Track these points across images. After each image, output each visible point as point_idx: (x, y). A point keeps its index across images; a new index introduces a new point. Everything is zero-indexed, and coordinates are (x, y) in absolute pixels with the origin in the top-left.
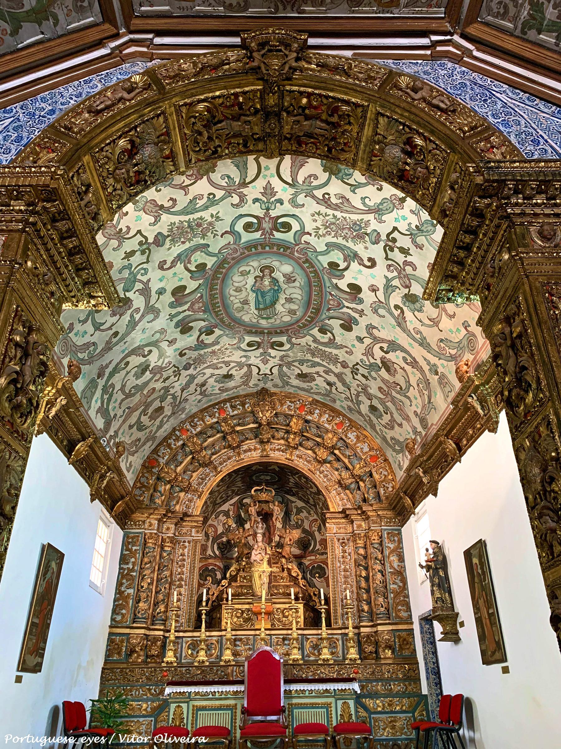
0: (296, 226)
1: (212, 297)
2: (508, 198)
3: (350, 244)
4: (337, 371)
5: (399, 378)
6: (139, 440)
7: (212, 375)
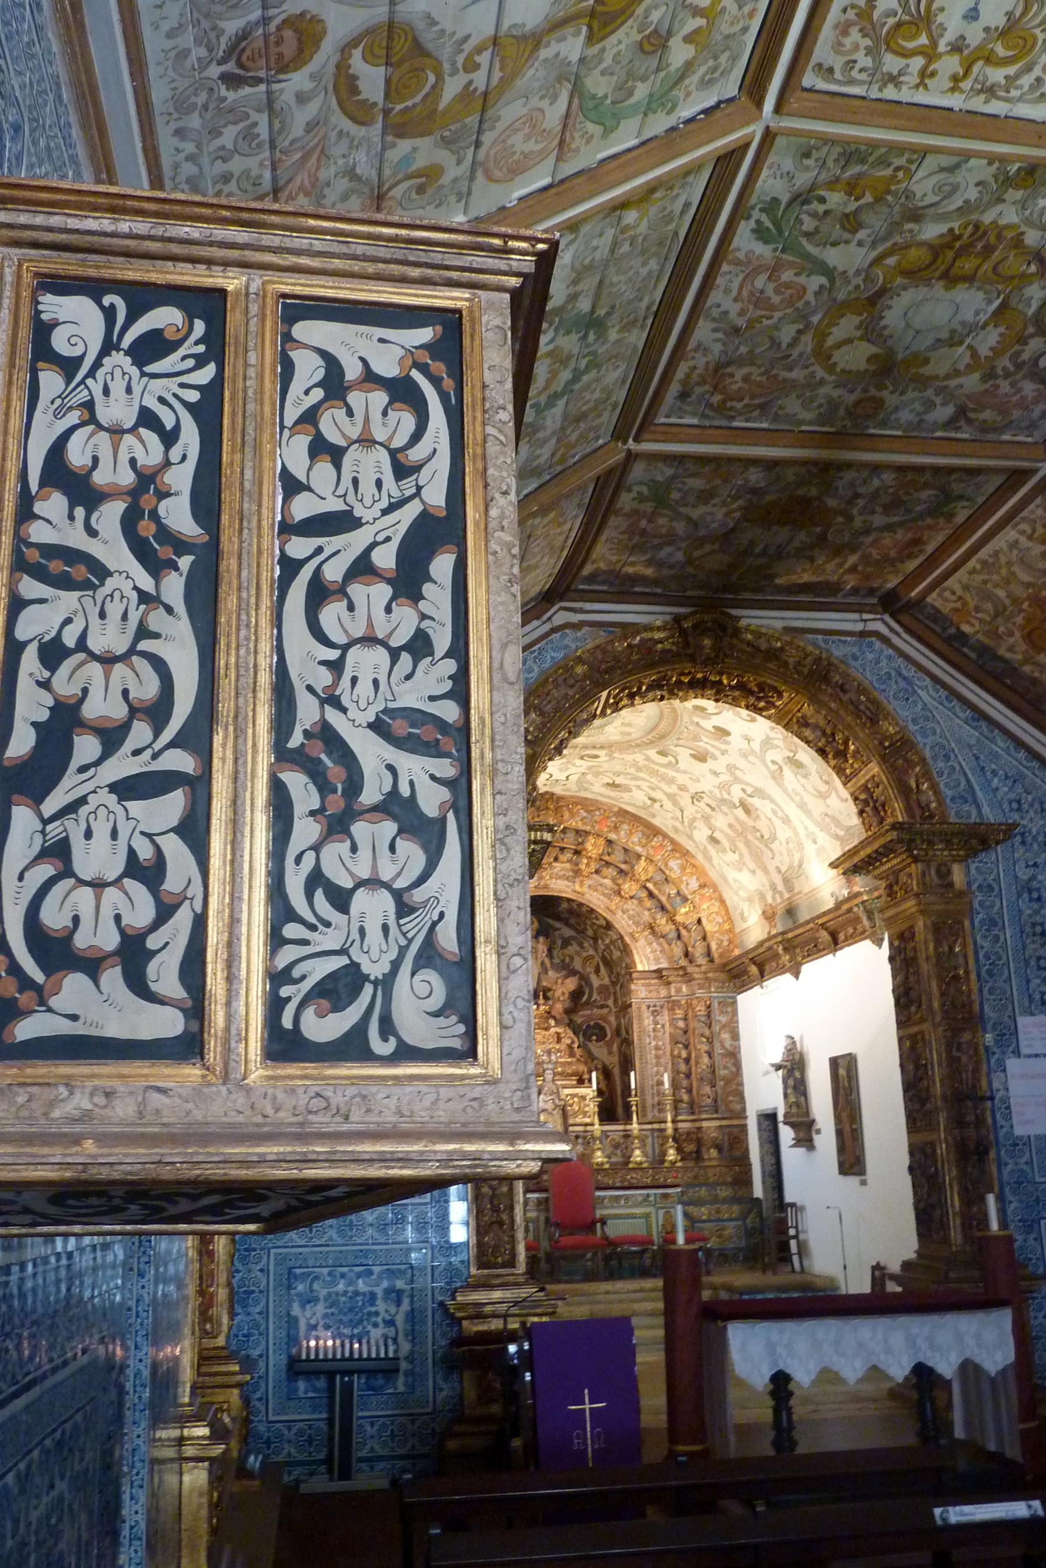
5: (763, 825)
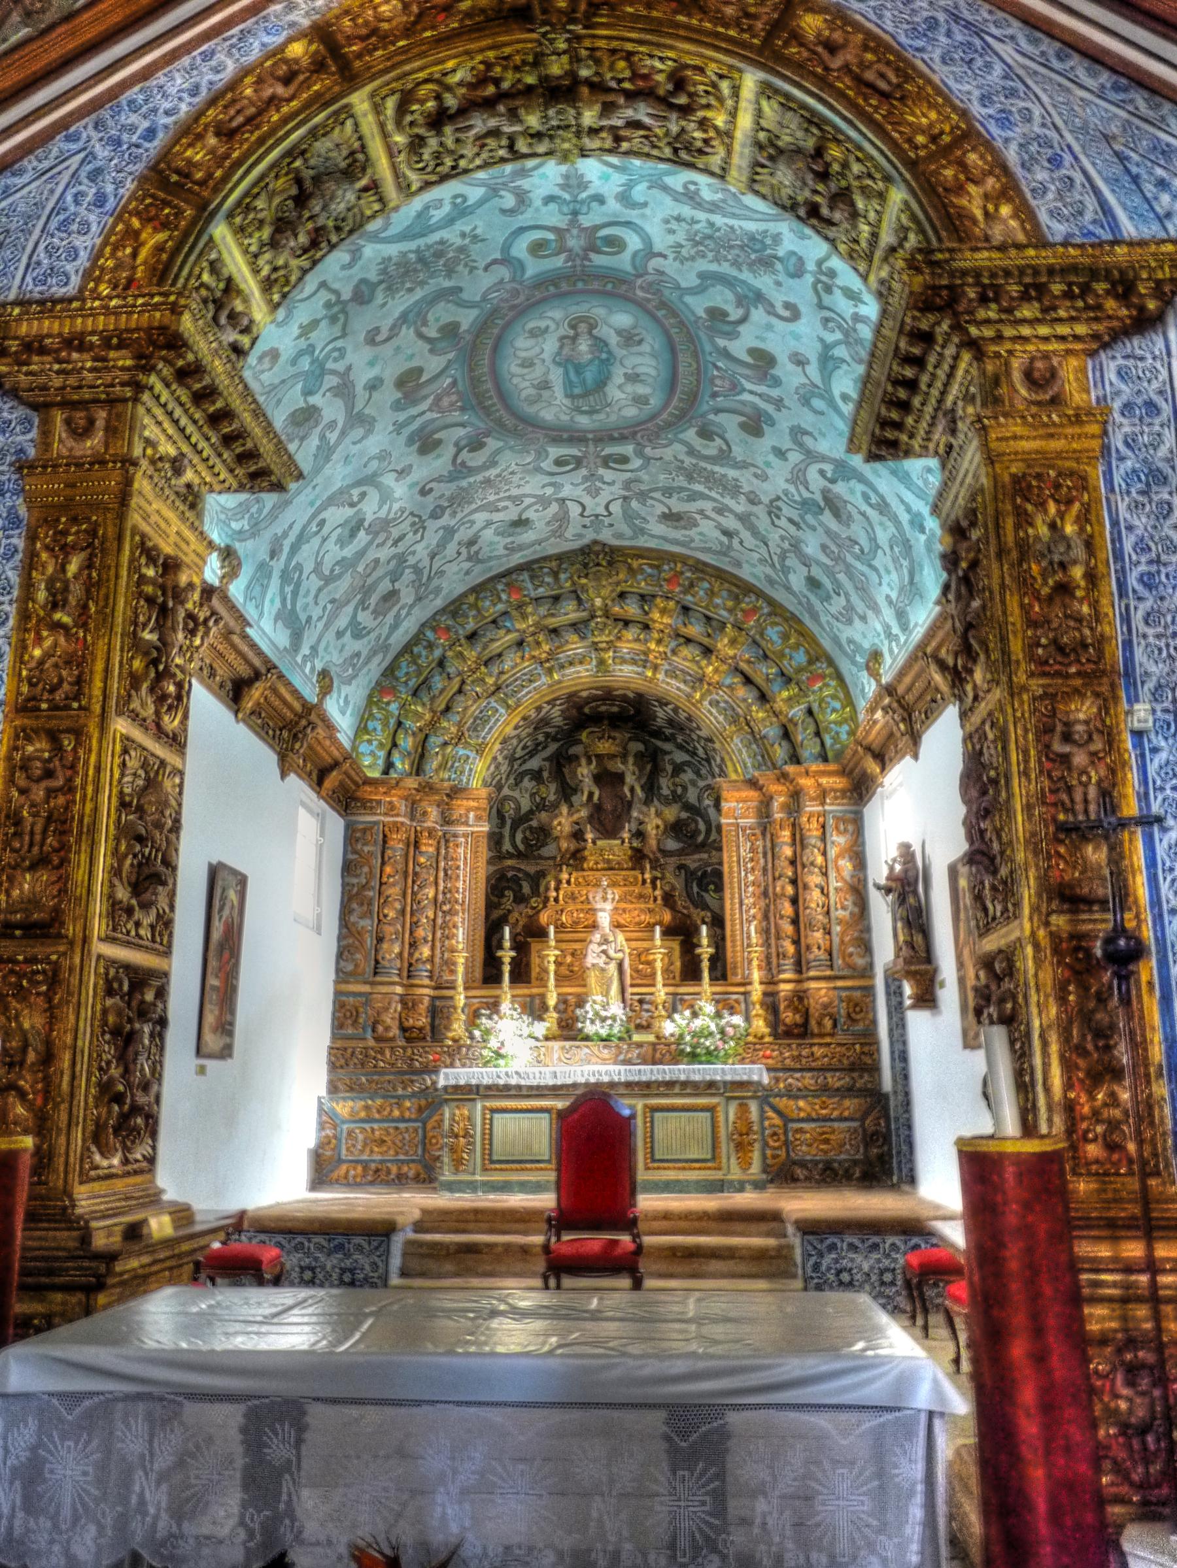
0: (634, 242)
1: (475, 382)
2: (971, 313)
3: (746, 275)
4: (740, 509)
5: (857, 530)
6: (358, 655)
7: (489, 523)
